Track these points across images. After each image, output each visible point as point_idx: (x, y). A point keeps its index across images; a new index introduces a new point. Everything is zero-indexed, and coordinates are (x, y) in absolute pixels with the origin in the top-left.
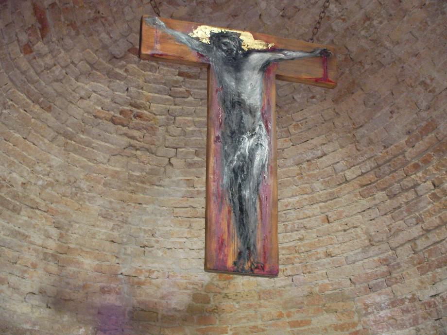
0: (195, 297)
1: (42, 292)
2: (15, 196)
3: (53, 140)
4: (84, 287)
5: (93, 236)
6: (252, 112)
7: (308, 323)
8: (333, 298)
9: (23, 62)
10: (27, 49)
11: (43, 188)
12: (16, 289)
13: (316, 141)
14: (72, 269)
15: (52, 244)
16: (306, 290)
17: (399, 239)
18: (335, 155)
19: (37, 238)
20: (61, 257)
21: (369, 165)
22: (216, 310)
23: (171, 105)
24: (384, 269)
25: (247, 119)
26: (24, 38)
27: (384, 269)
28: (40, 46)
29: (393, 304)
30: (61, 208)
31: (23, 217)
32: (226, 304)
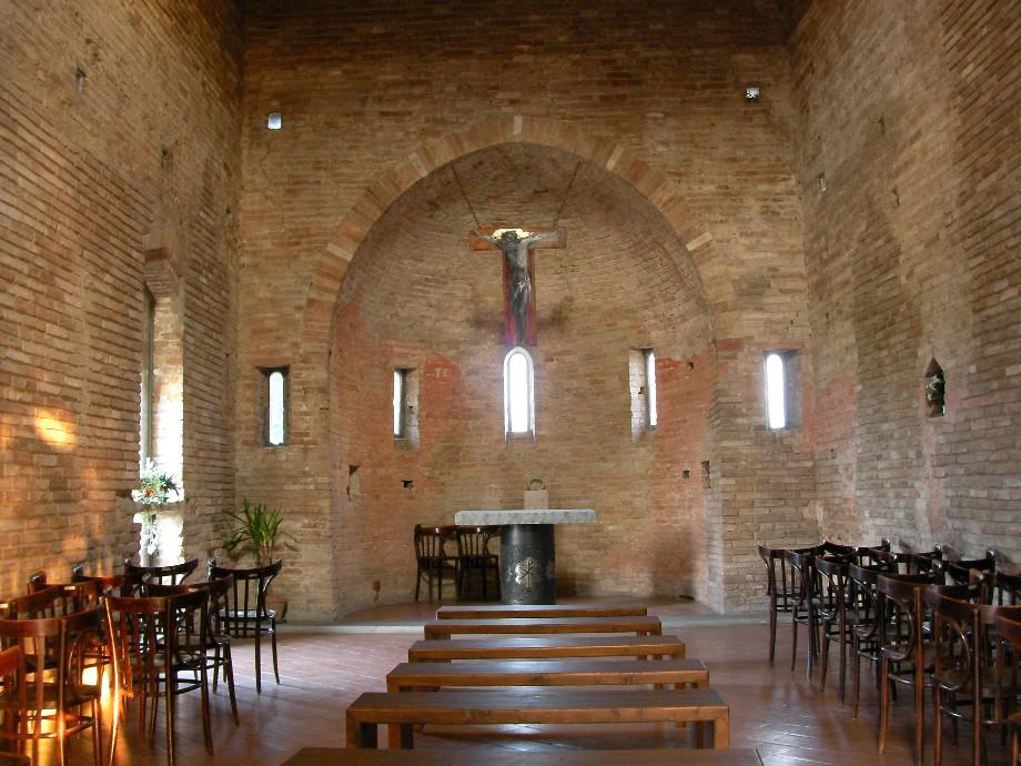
0: (555, 311)
1: (467, 320)
2: (443, 277)
3: (458, 245)
4: (491, 313)
5: (491, 285)
6: (523, 270)
7: (615, 324)
8: (627, 311)
9: (431, 221)
10: (431, 217)
11: (457, 270)
12: (452, 321)
13: (603, 229)
14: (482, 305)
15: (469, 295)
16: (612, 307)
17: (652, 284)
18: (614, 237)
19: (459, 294)
20: (475, 299)
21: (631, 244)
22: (566, 318)
23: (656, 58)
24: (648, 298)
25: (521, 275)
26: (427, 214)
27: (648, 298)
28: (437, 213)
29: (655, 317)
30: (470, 276)
31: (450, 285)
32: (572, 315)
